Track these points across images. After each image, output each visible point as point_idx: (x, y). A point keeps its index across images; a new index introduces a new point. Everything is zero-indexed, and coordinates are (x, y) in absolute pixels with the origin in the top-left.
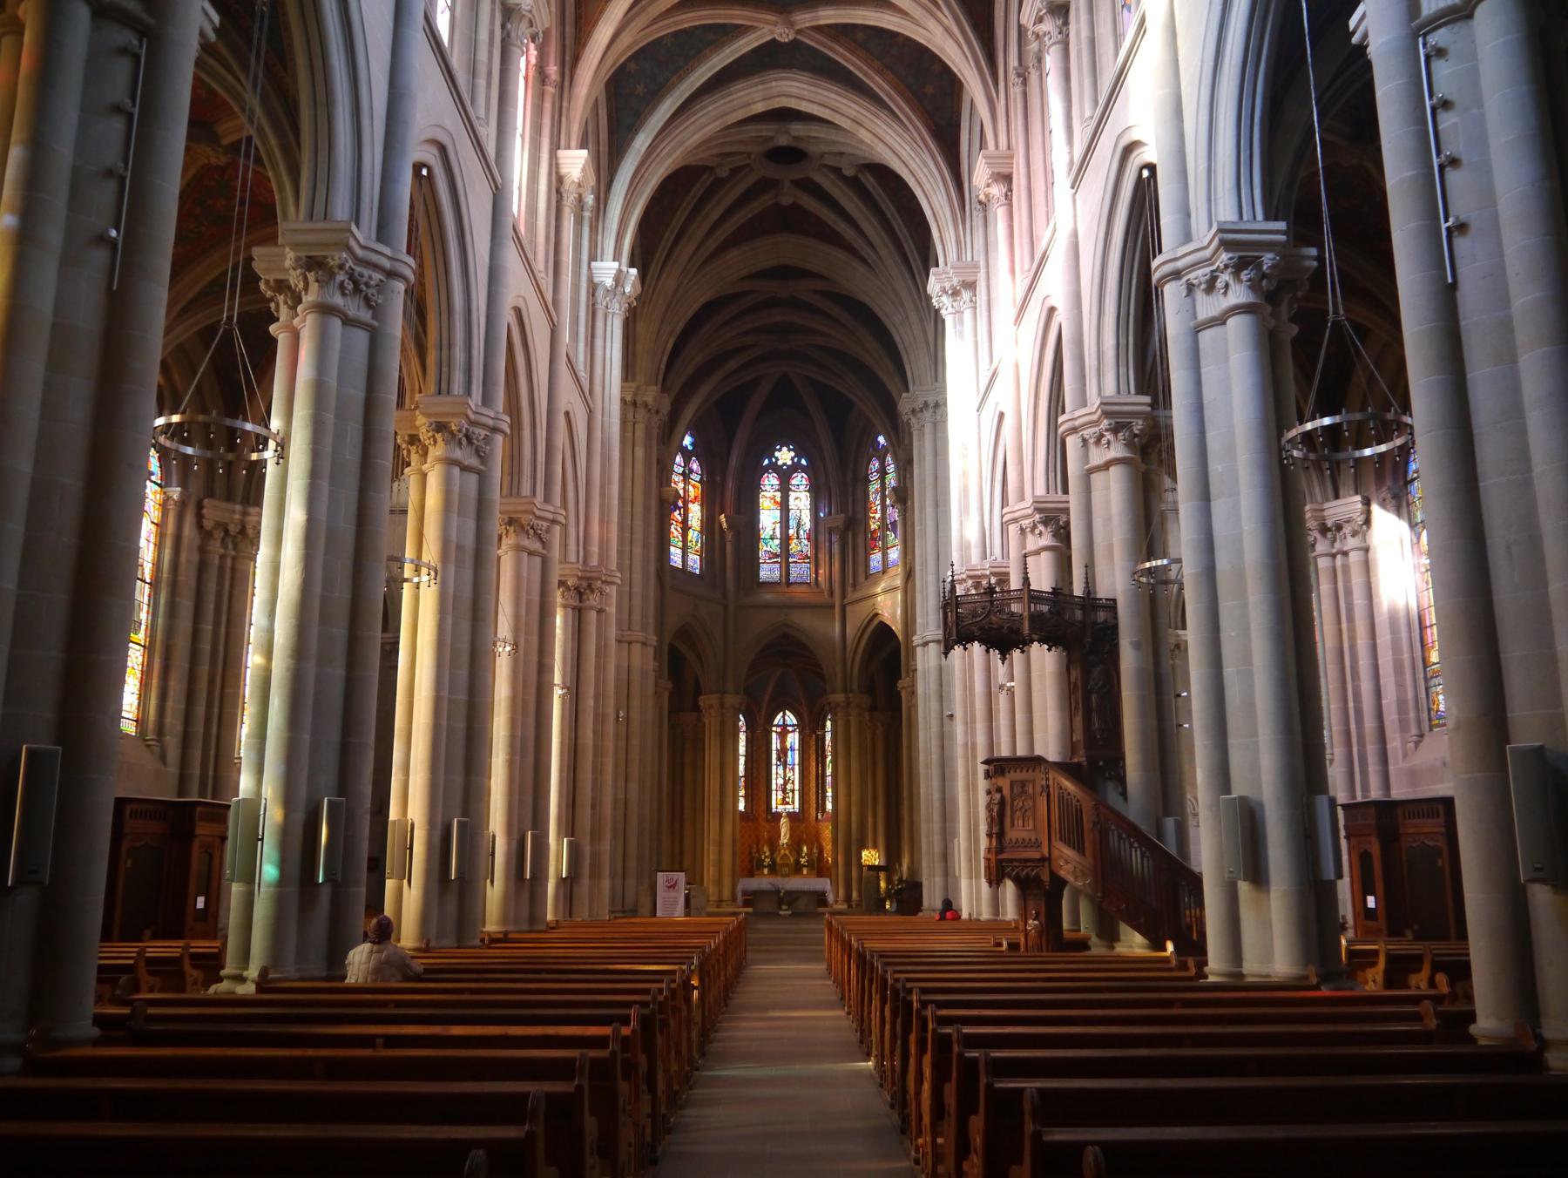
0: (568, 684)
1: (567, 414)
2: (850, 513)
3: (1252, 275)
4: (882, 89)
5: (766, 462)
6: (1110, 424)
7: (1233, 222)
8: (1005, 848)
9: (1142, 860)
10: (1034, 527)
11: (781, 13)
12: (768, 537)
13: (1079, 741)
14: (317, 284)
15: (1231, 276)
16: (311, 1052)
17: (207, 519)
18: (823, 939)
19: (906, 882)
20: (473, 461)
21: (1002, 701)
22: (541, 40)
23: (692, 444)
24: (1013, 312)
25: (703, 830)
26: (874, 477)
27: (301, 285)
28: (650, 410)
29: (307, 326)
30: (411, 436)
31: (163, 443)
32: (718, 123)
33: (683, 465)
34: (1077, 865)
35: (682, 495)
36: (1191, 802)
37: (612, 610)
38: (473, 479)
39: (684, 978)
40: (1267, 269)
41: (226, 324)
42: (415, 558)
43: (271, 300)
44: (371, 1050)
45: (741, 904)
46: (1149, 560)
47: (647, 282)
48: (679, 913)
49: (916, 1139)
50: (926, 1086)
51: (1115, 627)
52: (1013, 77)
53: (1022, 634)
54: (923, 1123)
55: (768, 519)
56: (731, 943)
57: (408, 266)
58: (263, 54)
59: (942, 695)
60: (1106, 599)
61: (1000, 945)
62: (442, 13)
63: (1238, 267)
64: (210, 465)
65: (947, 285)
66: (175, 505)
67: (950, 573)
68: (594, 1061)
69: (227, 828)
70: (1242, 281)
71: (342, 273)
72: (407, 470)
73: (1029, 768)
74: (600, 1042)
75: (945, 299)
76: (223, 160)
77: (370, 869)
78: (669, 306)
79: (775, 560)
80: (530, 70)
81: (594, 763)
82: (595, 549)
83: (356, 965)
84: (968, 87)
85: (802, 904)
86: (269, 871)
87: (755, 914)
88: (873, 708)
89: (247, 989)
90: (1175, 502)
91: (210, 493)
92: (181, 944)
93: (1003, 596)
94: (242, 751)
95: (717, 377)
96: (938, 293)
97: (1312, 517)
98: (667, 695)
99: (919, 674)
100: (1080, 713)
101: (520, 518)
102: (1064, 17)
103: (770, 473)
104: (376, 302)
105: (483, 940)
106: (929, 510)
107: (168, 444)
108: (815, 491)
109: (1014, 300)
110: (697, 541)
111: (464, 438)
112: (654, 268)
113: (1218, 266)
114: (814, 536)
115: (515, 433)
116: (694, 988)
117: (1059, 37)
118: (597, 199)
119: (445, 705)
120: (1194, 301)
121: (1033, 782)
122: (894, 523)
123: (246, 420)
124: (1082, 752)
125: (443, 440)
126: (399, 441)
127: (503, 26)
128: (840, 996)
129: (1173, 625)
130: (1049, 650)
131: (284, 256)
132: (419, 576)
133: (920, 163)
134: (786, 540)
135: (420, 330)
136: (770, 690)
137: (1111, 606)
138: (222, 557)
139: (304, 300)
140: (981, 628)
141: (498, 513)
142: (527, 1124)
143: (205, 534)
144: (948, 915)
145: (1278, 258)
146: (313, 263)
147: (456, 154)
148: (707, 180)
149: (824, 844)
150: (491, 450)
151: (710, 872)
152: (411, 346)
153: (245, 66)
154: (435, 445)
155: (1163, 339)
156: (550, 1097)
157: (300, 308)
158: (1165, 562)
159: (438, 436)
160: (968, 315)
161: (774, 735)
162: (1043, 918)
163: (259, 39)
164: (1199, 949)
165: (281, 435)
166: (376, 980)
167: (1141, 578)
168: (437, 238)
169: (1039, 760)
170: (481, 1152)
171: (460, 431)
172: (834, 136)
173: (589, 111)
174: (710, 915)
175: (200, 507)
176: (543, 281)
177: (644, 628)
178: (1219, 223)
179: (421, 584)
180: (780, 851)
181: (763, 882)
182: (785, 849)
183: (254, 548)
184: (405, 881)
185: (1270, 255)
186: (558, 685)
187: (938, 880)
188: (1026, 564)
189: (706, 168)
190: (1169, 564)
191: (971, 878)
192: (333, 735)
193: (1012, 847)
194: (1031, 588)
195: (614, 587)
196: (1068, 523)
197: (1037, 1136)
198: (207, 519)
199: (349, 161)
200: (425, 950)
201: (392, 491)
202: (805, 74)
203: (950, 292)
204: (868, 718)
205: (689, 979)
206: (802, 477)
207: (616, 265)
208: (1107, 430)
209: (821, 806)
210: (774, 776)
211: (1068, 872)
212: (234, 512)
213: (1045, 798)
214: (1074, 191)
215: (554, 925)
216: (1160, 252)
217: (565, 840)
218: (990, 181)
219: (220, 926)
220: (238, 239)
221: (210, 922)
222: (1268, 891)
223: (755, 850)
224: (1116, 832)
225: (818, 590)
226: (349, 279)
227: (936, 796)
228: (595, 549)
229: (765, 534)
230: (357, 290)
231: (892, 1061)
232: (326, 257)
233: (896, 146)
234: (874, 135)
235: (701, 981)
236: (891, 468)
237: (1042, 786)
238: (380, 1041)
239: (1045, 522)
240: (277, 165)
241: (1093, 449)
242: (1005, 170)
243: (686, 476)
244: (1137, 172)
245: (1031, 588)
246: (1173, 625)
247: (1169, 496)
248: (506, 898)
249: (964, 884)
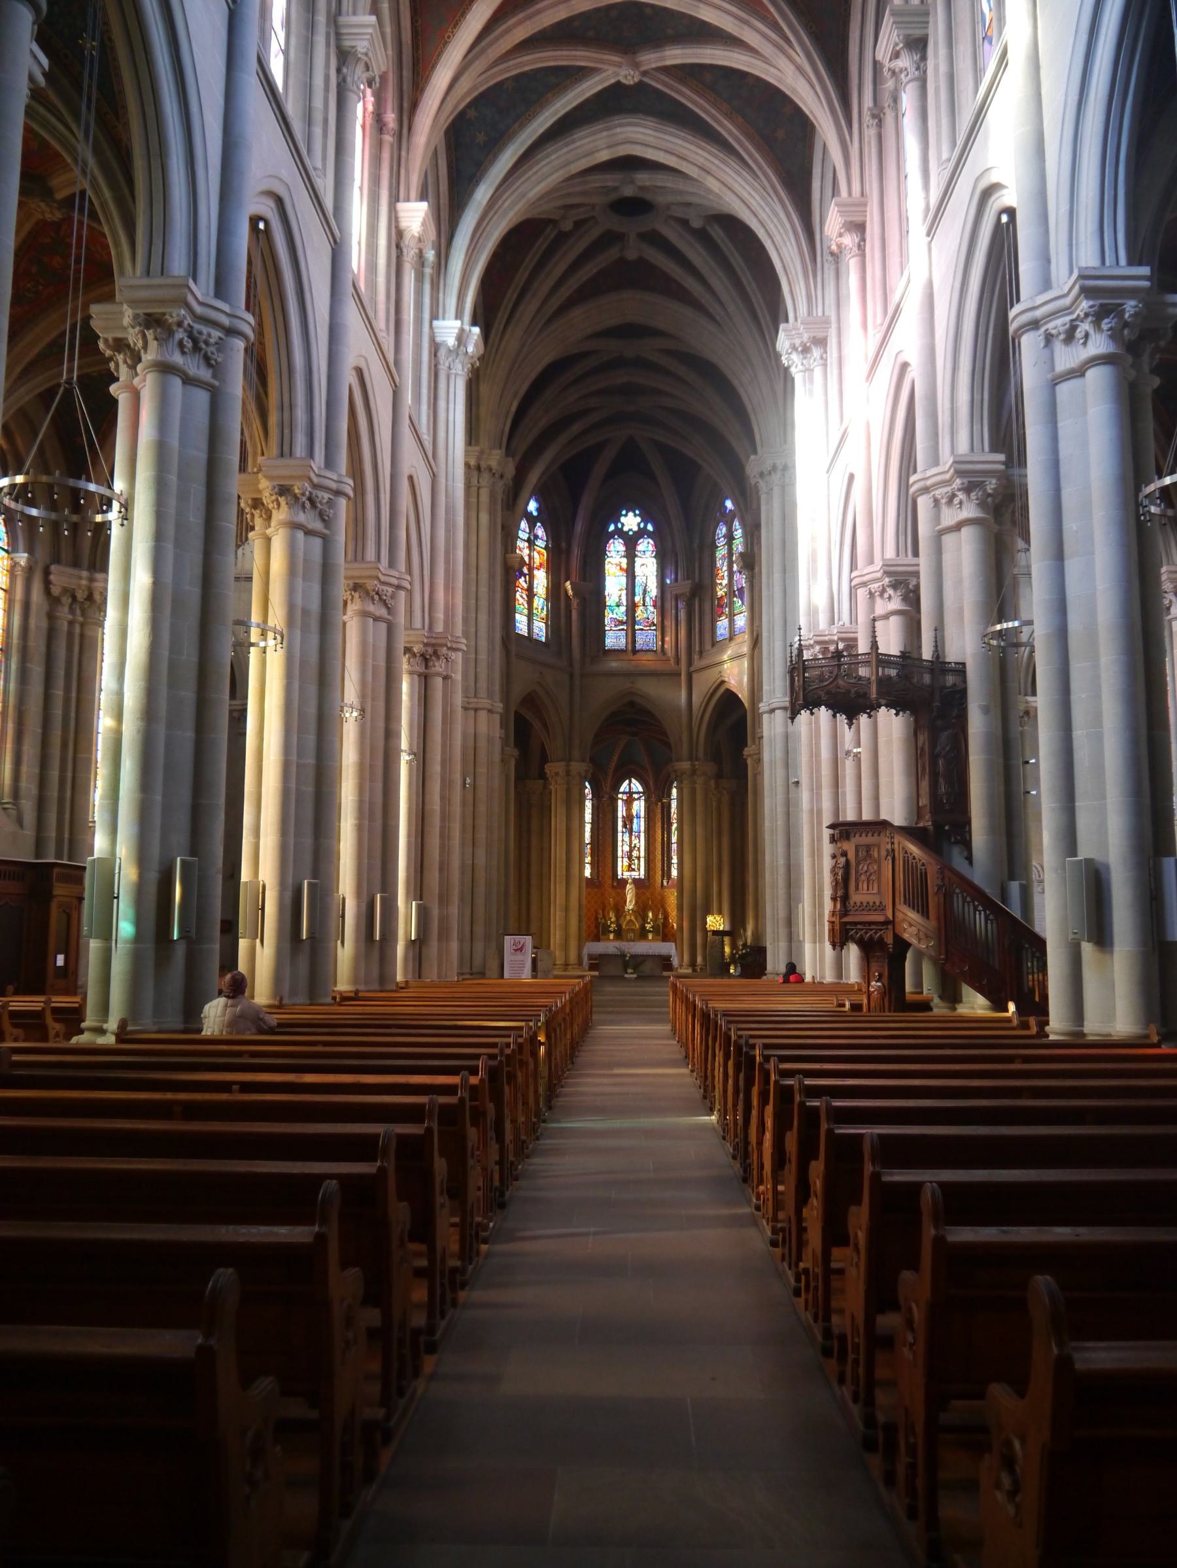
1: (411, 478)
2: (697, 580)
3: (1113, 324)
4: (730, 133)
5: (612, 528)
6: (963, 484)
7: (1094, 268)
8: (848, 911)
10: (883, 591)
11: (626, 53)
12: (614, 604)
13: (926, 806)
14: (155, 342)
15: (1092, 325)
16: (169, 1096)
17: (55, 585)
18: (669, 1001)
19: (750, 947)
20: (318, 525)
21: (849, 766)
22: (378, 85)
23: (538, 510)
24: (866, 368)
25: (550, 859)
26: (721, 542)
27: (140, 344)
28: (494, 474)
29: (148, 385)
30: (254, 500)
31: (7, 504)
32: (561, 172)
33: (528, 530)
34: (921, 928)
35: (528, 562)
36: (1036, 868)
37: (458, 677)
38: (317, 542)
39: (531, 1034)
40: (1129, 317)
41: (66, 382)
42: (260, 622)
44: (227, 1094)
45: (587, 968)
46: (1000, 622)
47: (492, 336)
48: (526, 975)
49: (757, 1187)
50: (768, 1136)
51: (964, 692)
52: (868, 118)
53: (869, 698)
54: (765, 1172)
55: (614, 585)
56: (577, 1003)
57: (247, 323)
59: (788, 762)
60: (956, 663)
61: (844, 1005)
62: (276, 56)
63: (1099, 316)
64: (55, 527)
65: (797, 342)
66: (23, 571)
67: (797, 638)
68: (443, 1107)
69: (84, 889)
70: (1103, 331)
71: (181, 330)
72: (251, 534)
73: (874, 832)
74: (450, 1090)
75: (794, 356)
76: (58, 215)
77: (223, 931)
79: (621, 627)
80: (367, 118)
81: (442, 828)
82: (440, 615)
83: (212, 1019)
84: (821, 133)
85: (647, 968)
86: (125, 928)
87: (601, 977)
88: (719, 776)
89: (109, 1040)
90: (1029, 567)
91: (56, 559)
92: (43, 999)
93: (851, 660)
94: (96, 815)
95: (563, 439)
96: (787, 350)
97: (1168, 579)
99: (765, 741)
100: (927, 777)
101: (364, 584)
102: (921, 52)
103: (615, 539)
104: (216, 361)
105: (334, 998)
106: (777, 576)
107: (13, 505)
108: (662, 557)
109: (866, 356)
110: (543, 609)
111: (307, 502)
112: (498, 326)
113: (1078, 315)
114: (661, 604)
115: (359, 497)
116: (541, 1044)
117: (916, 73)
118: (438, 255)
119: (294, 769)
121: (879, 847)
122: (741, 590)
123: (89, 480)
124: (928, 817)
125: (287, 504)
126: (242, 505)
127: (339, 71)
128: (684, 1054)
129: (1022, 691)
130: (897, 714)
131: (122, 313)
132: (265, 640)
134: (632, 607)
135: (261, 390)
136: (615, 758)
137: (960, 670)
138: (71, 623)
139: (143, 359)
140: (828, 693)
141: (343, 579)
142: (379, 1161)
143: (53, 601)
144: (792, 978)
145: (1140, 305)
146: (151, 321)
147: (294, 206)
148: (550, 234)
149: (669, 911)
150: (335, 514)
151: (556, 937)
152: (252, 407)
153: (77, 116)
155: (1019, 395)
156: (401, 1138)
157: (139, 367)
158: (1016, 624)
159: (282, 500)
160: (818, 372)
161: (620, 802)
162: (885, 979)
163: (90, 86)
164: (1041, 1010)
165: (125, 496)
166: (231, 1033)
167: (991, 641)
169: (885, 824)
170: (334, 1182)
171: (303, 494)
172: (680, 185)
173: (428, 161)
174: (556, 977)
175: (47, 573)
176: (384, 340)
177: (490, 695)
178: (1080, 269)
179: (268, 649)
180: (625, 917)
181: (609, 946)
182: (630, 915)
183: (102, 614)
184: (258, 941)
185: (1133, 303)
186: (405, 751)
187: (783, 945)
188: (874, 627)
189: (549, 221)
190: (1020, 626)
191: (815, 943)
192: (184, 794)
193: (857, 910)
194: (880, 651)
195: (460, 654)
196: (917, 587)
197: (875, 1177)
198: (55, 585)
199: (185, 213)
200: (279, 1006)
201: (236, 558)
202: (650, 119)
203: (800, 349)
204: (713, 786)
205: (535, 1035)
206: (648, 543)
207: (458, 323)
208: (959, 490)
209: (666, 873)
210: (620, 843)
211: (911, 935)
212: (80, 578)
213: (890, 861)
214: (930, 239)
215: (403, 985)
216: (1018, 300)
217: (414, 903)
218: (842, 231)
219: (80, 983)
220: (75, 298)
221: (70, 978)
222: (1112, 952)
223: (600, 916)
224: (960, 895)
225: (664, 658)
227: (781, 862)
228: (440, 615)
229: (611, 601)
230: (196, 348)
231: (735, 1115)
232: (164, 314)
233: (745, 195)
234: (722, 183)
235: (548, 1037)
236: (738, 533)
237: (887, 850)
238: (235, 1087)
239: (895, 586)
240: (112, 219)
241: (945, 510)
242: (858, 219)
243: (531, 542)
244: (995, 218)
245: (880, 651)
246: (1022, 691)
247: (1021, 557)
248: (357, 959)
249: (808, 947)
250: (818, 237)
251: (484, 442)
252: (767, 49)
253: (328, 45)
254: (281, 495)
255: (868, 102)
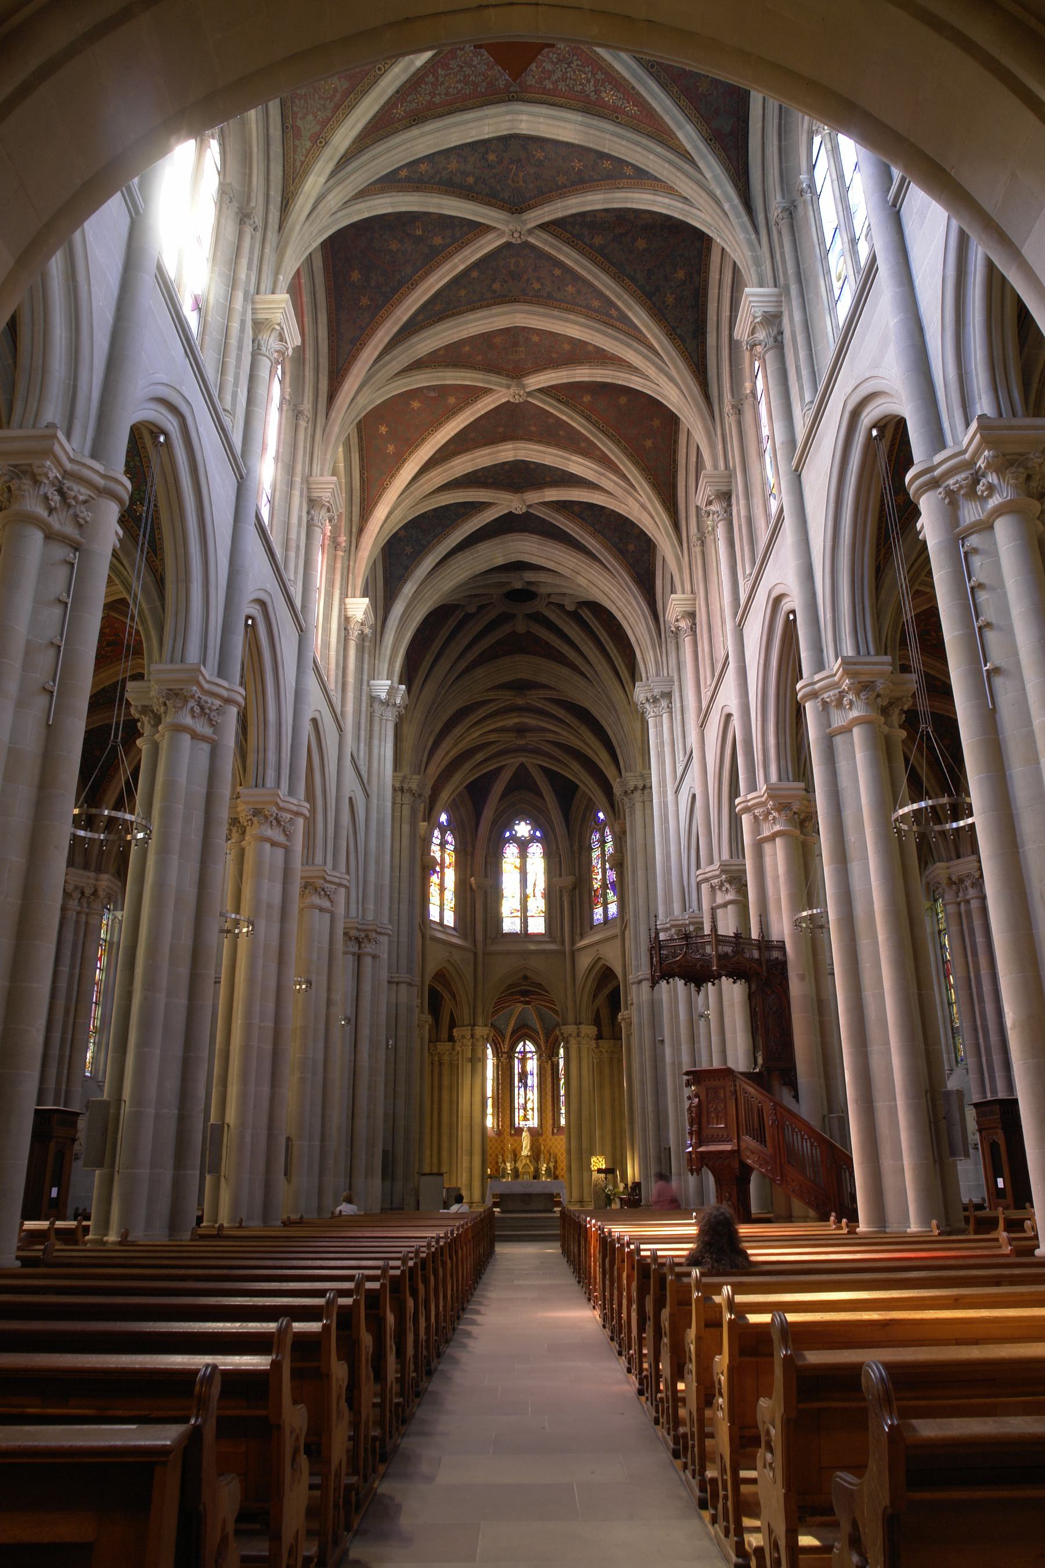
0: (349, 1015)
5: (508, 834)
9: (812, 1149)
20: (281, 838)
23: (447, 820)
26: (596, 845)
33: (440, 837)
38: (280, 853)
43: (138, 720)
57: (239, 693)
58: (145, 552)
65: (649, 695)
75: (647, 706)
78: (429, 712)
88: (599, 1037)
95: (468, 765)
98: (427, 1027)
108: (548, 855)
120: (828, 714)
127: (308, 513)
130: (734, 982)
133: (625, 602)
138: (78, 913)
148: (459, 615)
154: (252, 825)
157: (160, 728)
161: (516, 1061)
168: (257, 666)
172: (557, 581)
177: (410, 970)
189: (457, 606)
194: (720, 933)
207: (389, 682)
210: (516, 1097)
223: (500, 1160)
226: (198, 705)
237: (731, 1091)
243: (443, 845)
250: (661, 619)
251: (406, 770)
252: (619, 492)
253: (301, 496)
254: (254, 816)
255: (693, 530)
